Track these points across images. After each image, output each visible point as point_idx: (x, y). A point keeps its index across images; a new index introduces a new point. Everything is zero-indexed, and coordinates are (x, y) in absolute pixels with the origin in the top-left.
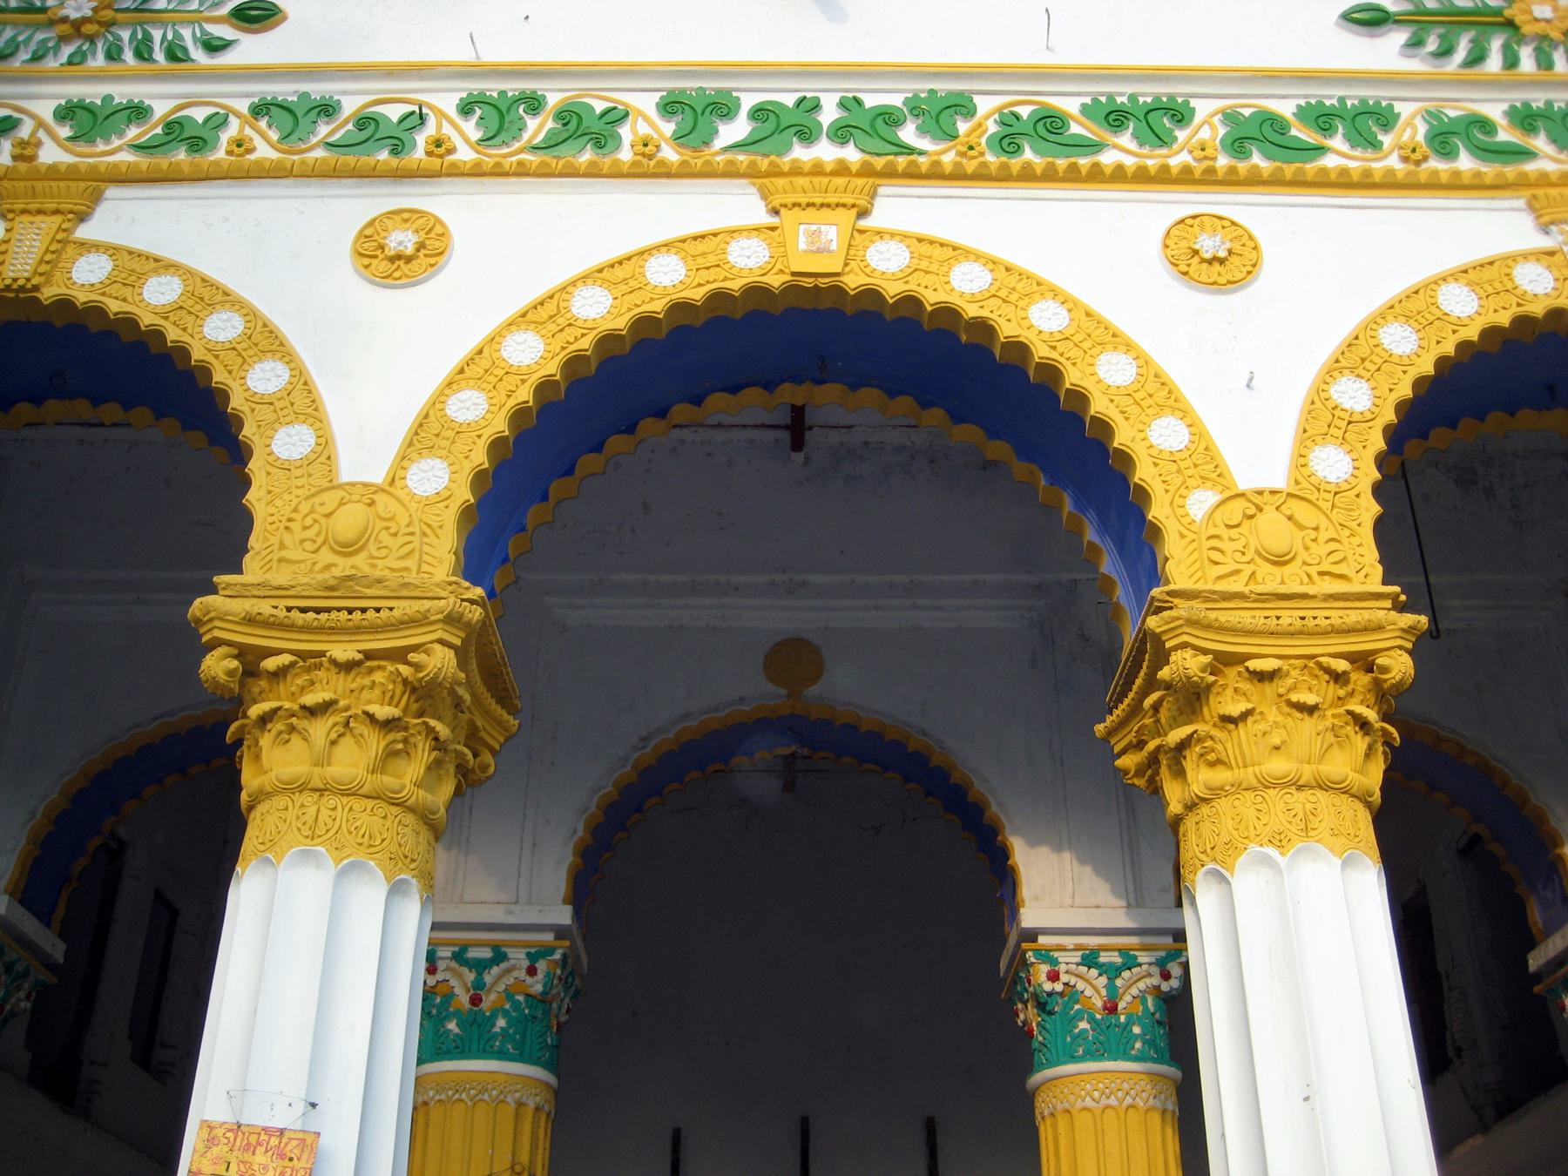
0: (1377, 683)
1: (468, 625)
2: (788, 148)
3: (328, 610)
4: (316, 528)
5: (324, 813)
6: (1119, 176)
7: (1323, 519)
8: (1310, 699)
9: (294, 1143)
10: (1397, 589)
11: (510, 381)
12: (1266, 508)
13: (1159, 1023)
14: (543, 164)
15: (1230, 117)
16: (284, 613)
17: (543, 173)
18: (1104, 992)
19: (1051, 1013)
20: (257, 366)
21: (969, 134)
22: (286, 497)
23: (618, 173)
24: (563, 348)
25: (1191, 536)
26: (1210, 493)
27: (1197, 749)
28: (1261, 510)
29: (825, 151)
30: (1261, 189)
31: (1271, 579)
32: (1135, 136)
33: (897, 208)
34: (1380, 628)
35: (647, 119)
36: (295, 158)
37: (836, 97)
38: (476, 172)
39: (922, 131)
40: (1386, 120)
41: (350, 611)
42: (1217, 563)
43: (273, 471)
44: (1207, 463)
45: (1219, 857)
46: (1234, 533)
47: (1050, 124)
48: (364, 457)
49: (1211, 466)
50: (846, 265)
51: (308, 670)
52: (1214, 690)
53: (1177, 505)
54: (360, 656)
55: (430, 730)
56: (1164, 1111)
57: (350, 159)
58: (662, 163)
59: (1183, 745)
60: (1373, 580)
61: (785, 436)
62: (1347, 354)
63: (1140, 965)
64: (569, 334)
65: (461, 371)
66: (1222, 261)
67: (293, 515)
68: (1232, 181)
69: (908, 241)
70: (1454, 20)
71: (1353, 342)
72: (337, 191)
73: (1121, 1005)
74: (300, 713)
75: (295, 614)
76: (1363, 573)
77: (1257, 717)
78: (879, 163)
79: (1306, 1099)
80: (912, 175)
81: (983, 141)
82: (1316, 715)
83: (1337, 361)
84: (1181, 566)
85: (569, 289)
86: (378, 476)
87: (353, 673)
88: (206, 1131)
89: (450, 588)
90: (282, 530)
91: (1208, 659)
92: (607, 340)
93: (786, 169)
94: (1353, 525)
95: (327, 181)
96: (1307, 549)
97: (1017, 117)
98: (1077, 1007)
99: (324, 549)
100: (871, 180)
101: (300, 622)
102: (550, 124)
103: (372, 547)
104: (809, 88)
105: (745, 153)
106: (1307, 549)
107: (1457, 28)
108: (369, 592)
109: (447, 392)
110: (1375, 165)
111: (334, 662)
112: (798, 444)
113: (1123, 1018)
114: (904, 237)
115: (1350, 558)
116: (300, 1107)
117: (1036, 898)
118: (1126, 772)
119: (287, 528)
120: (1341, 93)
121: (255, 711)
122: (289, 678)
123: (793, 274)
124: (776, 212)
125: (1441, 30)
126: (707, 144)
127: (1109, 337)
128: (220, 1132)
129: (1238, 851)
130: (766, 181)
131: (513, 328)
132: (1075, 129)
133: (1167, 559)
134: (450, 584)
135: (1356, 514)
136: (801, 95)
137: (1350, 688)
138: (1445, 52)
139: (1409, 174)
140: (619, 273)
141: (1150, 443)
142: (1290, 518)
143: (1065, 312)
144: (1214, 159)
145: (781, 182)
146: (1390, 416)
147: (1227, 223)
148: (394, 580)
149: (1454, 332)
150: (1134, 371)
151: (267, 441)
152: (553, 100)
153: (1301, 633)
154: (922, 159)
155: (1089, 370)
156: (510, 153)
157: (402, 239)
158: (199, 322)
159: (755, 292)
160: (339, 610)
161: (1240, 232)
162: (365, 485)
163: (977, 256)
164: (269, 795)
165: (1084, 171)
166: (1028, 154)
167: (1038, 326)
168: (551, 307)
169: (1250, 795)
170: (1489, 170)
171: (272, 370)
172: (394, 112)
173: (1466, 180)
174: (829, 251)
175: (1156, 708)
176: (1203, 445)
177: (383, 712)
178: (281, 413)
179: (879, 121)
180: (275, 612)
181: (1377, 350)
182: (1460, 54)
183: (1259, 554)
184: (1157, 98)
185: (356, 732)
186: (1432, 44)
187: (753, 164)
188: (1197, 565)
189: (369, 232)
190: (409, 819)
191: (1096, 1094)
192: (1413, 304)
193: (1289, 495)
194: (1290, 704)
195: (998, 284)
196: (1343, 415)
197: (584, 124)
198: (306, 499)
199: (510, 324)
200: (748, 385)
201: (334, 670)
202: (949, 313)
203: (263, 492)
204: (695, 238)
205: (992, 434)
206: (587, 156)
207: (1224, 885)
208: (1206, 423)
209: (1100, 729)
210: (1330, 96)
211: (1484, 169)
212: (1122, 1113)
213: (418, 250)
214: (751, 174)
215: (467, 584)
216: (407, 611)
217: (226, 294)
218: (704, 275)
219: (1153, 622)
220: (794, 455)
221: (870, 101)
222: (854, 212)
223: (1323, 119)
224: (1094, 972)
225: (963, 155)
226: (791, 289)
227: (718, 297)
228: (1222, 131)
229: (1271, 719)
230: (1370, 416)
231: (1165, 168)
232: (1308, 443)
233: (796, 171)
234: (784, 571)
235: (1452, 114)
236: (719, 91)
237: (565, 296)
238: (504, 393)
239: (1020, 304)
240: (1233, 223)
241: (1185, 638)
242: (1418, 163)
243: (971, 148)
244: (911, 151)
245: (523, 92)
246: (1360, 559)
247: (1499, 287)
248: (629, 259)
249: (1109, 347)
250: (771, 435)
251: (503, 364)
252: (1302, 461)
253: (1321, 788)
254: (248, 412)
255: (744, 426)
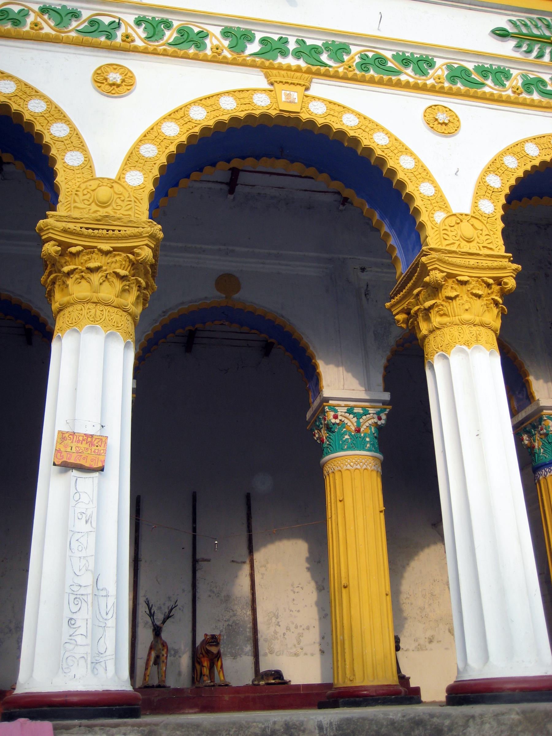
0: (502, 290)
1: (158, 239)
2: (275, 58)
3: (98, 229)
4: (89, 195)
5: (98, 312)
6: (407, 86)
7: (484, 227)
8: (480, 292)
9: (97, 440)
10: (511, 255)
11: (166, 143)
12: (464, 221)
13: (376, 437)
14: (175, 52)
15: (449, 67)
16: (79, 229)
17: (174, 55)
18: (355, 424)
19: (333, 432)
20: (54, 125)
21: (348, 61)
22: (73, 181)
23: (205, 60)
24: (188, 131)
25: (436, 229)
26: (442, 213)
27: (436, 309)
28: (461, 221)
29: (291, 61)
30: (460, 97)
31: (466, 247)
32: (413, 70)
33: (320, 88)
34: (505, 268)
35: (216, 38)
36: (63, 35)
37: (295, 39)
38: (145, 52)
39: (330, 57)
40: (508, 76)
41: (108, 230)
42: (446, 240)
43: (67, 170)
44: (441, 202)
45: (444, 349)
46: (452, 229)
47: (380, 61)
48: (107, 165)
49: (443, 203)
50: (301, 109)
51: (88, 254)
52: (444, 287)
53: (431, 217)
54: (111, 249)
55: (138, 282)
56: (378, 471)
57: (89, 38)
58: (225, 57)
59: (431, 307)
60: (502, 251)
61: (225, 188)
62: (492, 166)
63: (370, 414)
64: (190, 125)
65: (145, 136)
66: (446, 124)
67: (78, 189)
68: (450, 93)
69: (325, 102)
70: (534, 39)
71: (494, 161)
72: (82, 52)
73: (362, 430)
74: (86, 271)
75: (83, 230)
76: (498, 248)
77: (460, 298)
78: (314, 68)
79: (477, 435)
80: (327, 75)
81: (354, 64)
82: (481, 299)
83: (488, 168)
84: (433, 239)
85: (189, 106)
86: (113, 176)
87: (108, 256)
88: (60, 434)
89: (149, 224)
90: (74, 195)
91: (445, 274)
92: (205, 129)
93: (276, 66)
94: (494, 230)
95: (79, 47)
96: (478, 237)
97: (367, 56)
98: (344, 430)
99: (93, 204)
100: (311, 76)
101: (86, 233)
102: (175, 35)
103: (114, 205)
104: (284, 33)
105: (258, 58)
106: (478, 237)
107: (534, 42)
108: (115, 223)
109: (140, 144)
110: (503, 93)
111: (100, 251)
112: (232, 191)
113: (362, 435)
114: (324, 100)
115: (494, 242)
116: (99, 427)
117: (328, 386)
118: (398, 321)
119: (76, 194)
120: (491, 63)
121: (66, 269)
122: (80, 256)
123: (281, 110)
124: (272, 84)
125: (528, 42)
126: (243, 52)
127: (404, 150)
128: (67, 435)
129: (452, 347)
130: (268, 70)
131: (166, 120)
132: (390, 64)
133: (427, 237)
134: (149, 222)
135: (495, 226)
136: (281, 36)
137: (492, 290)
138: (529, 52)
139: (516, 98)
140: (209, 102)
141: (421, 192)
142: (472, 225)
143: (387, 138)
144: (443, 83)
145: (275, 72)
146: (507, 191)
147: (448, 110)
148: (125, 219)
149: (531, 161)
150: (414, 164)
151: (63, 157)
152: (176, 24)
153: (477, 268)
154: (330, 69)
155: (397, 161)
156: (158, 45)
157: (115, 77)
158: (25, 103)
159: (265, 116)
160: (103, 229)
161: (453, 114)
162: (109, 179)
163: (353, 112)
164: (72, 304)
165: (394, 82)
166: (372, 72)
167: (378, 142)
168: (181, 113)
169: (456, 327)
170: (545, 100)
171: (62, 127)
172: (106, 20)
173: (536, 103)
174: (294, 103)
175: (418, 294)
176: (440, 195)
177: (123, 272)
178: (67, 146)
179: (313, 51)
180: (75, 228)
181: (503, 165)
182: (535, 54)
183: (461, 237)
184: (421, 55)
185: (111, 280)
186: (525, 48)
187: (263, 62)
188: (439, 240)
189: (99, 72)
190: (129, 318)
191: (352, 464)
192: (516, 149)
193: (472, 217)
194: (473, 294)
195: (361, 124)
196: (491, 188)
197: (190, 37)
198: (84, 183)
199: (164, 118)
200: (249, 157)
201: (100, 254)
202: (342, 133)
203: (63, 179)
204: (239, 91)
205: (348, 186)
206: (192, 51)
207: (445, 360)
208: (441, 186)
209: (388, 304)
210: (487, 63)
211: (543, 100)
212: (362, 471)
213: (122, 83)
214: (261, 67)
215: (155, 223)
216: (133, 232)
217: (37, 92)
218: (244, 107)
219: (424, 259)
220: (229, 196)
221: (309, 42)
222: (304, 87)
223: (484, 72)
224: (351, 416)
225: (347, 69)
226: (279, 117)
227: (250, 117)
228: (446, 73)
229: (465, 299)
230: (500, 190)
231: (425, 84)
232: (478, 198)
233: (280, 68)
234: (225, 245)
235: (532, 76)
236: (246, 30)
237: (186, 109)
238: (164, 147)
239: (370, 132)
240: (450, 110)
241: (436, 266)
242: (519, 94)
243: (350, 67)
244: (325, 65)
245: (162, 19)
246: (497, 243)
247: (547, 146)
248: (212, 96)
249: (404, 153)
250: (219, 186)
251: (162, 135)
252: (476, 204)
253: (482, 325)
254: (52, 144)
255: (209, 181)
